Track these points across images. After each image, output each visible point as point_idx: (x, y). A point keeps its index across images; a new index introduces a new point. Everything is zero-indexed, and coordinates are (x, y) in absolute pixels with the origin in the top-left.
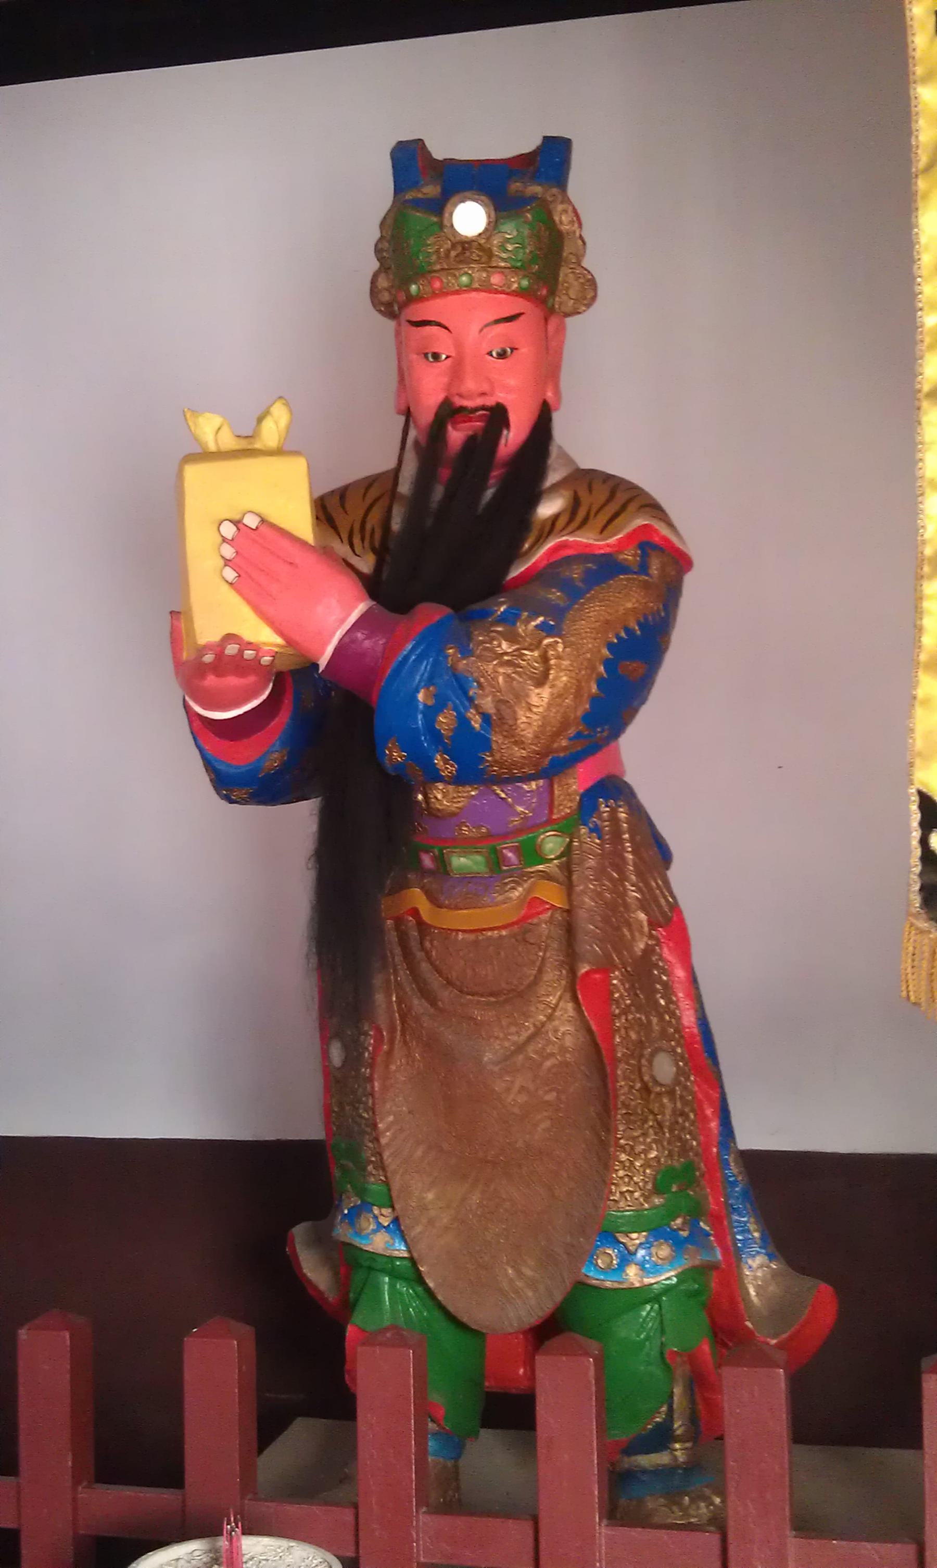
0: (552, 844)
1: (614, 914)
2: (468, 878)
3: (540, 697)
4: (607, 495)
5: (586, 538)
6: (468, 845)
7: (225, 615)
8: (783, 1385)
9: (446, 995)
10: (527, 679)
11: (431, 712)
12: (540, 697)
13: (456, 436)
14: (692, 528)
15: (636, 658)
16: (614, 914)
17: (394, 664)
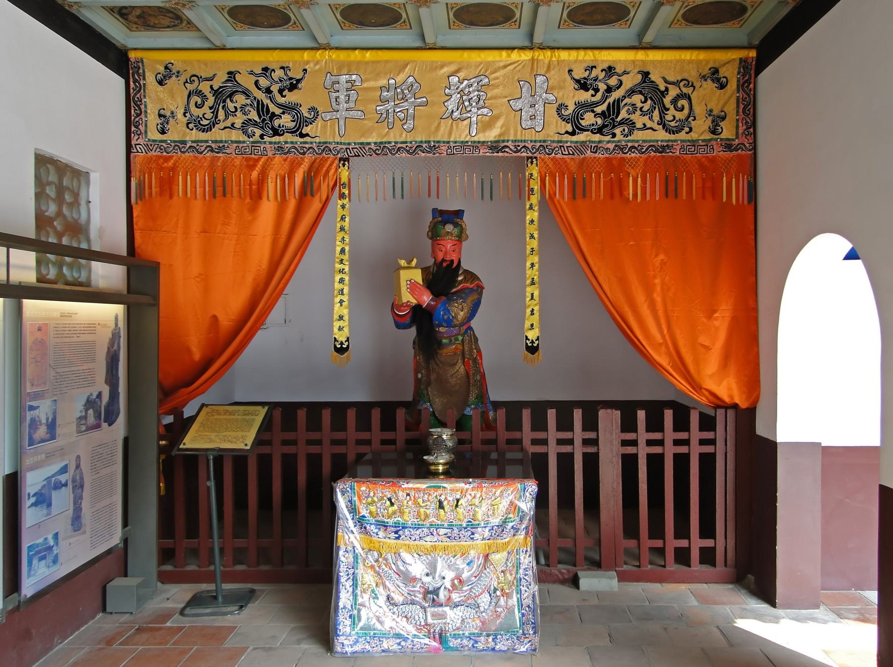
0: (460, 338)
1: (471, 350)
2: (446, 344)
3: (462, 313)
4: (471, 276)
5: (468, 285)
6: (446, 338)
7: (407, 297)
8: (292, 38)
9: (441, 365)
10: (459, 311)
11: (443, 316)
12: (462, 313)
13: (444, 264)
14: (485, 283)
15: (476, 306)
16: (471, 350)
17: (325, 169)
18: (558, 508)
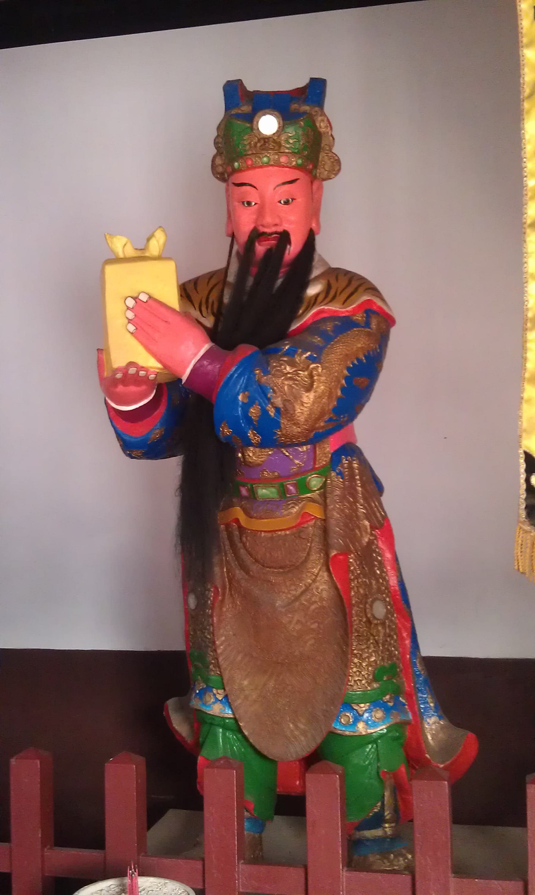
0: (315, 482)
1: (351, 522)
2: (267, 501)
3: (309, 398)
4: (347, 283)
5: (334, 307)
6: (267, 482)
7: (129, 351)
9: (254, 568)
10: (301, 388)
11: (246, 407)
12: (309, 398)
13: (260, 249)
14: (395, 302)
15: (363, 375)
16: (351, 522)
18: (104, 819)
